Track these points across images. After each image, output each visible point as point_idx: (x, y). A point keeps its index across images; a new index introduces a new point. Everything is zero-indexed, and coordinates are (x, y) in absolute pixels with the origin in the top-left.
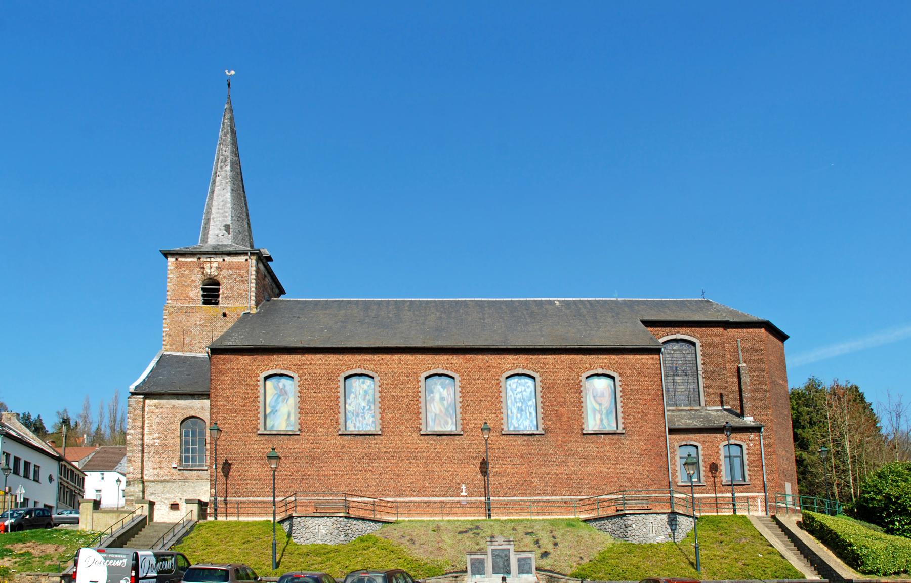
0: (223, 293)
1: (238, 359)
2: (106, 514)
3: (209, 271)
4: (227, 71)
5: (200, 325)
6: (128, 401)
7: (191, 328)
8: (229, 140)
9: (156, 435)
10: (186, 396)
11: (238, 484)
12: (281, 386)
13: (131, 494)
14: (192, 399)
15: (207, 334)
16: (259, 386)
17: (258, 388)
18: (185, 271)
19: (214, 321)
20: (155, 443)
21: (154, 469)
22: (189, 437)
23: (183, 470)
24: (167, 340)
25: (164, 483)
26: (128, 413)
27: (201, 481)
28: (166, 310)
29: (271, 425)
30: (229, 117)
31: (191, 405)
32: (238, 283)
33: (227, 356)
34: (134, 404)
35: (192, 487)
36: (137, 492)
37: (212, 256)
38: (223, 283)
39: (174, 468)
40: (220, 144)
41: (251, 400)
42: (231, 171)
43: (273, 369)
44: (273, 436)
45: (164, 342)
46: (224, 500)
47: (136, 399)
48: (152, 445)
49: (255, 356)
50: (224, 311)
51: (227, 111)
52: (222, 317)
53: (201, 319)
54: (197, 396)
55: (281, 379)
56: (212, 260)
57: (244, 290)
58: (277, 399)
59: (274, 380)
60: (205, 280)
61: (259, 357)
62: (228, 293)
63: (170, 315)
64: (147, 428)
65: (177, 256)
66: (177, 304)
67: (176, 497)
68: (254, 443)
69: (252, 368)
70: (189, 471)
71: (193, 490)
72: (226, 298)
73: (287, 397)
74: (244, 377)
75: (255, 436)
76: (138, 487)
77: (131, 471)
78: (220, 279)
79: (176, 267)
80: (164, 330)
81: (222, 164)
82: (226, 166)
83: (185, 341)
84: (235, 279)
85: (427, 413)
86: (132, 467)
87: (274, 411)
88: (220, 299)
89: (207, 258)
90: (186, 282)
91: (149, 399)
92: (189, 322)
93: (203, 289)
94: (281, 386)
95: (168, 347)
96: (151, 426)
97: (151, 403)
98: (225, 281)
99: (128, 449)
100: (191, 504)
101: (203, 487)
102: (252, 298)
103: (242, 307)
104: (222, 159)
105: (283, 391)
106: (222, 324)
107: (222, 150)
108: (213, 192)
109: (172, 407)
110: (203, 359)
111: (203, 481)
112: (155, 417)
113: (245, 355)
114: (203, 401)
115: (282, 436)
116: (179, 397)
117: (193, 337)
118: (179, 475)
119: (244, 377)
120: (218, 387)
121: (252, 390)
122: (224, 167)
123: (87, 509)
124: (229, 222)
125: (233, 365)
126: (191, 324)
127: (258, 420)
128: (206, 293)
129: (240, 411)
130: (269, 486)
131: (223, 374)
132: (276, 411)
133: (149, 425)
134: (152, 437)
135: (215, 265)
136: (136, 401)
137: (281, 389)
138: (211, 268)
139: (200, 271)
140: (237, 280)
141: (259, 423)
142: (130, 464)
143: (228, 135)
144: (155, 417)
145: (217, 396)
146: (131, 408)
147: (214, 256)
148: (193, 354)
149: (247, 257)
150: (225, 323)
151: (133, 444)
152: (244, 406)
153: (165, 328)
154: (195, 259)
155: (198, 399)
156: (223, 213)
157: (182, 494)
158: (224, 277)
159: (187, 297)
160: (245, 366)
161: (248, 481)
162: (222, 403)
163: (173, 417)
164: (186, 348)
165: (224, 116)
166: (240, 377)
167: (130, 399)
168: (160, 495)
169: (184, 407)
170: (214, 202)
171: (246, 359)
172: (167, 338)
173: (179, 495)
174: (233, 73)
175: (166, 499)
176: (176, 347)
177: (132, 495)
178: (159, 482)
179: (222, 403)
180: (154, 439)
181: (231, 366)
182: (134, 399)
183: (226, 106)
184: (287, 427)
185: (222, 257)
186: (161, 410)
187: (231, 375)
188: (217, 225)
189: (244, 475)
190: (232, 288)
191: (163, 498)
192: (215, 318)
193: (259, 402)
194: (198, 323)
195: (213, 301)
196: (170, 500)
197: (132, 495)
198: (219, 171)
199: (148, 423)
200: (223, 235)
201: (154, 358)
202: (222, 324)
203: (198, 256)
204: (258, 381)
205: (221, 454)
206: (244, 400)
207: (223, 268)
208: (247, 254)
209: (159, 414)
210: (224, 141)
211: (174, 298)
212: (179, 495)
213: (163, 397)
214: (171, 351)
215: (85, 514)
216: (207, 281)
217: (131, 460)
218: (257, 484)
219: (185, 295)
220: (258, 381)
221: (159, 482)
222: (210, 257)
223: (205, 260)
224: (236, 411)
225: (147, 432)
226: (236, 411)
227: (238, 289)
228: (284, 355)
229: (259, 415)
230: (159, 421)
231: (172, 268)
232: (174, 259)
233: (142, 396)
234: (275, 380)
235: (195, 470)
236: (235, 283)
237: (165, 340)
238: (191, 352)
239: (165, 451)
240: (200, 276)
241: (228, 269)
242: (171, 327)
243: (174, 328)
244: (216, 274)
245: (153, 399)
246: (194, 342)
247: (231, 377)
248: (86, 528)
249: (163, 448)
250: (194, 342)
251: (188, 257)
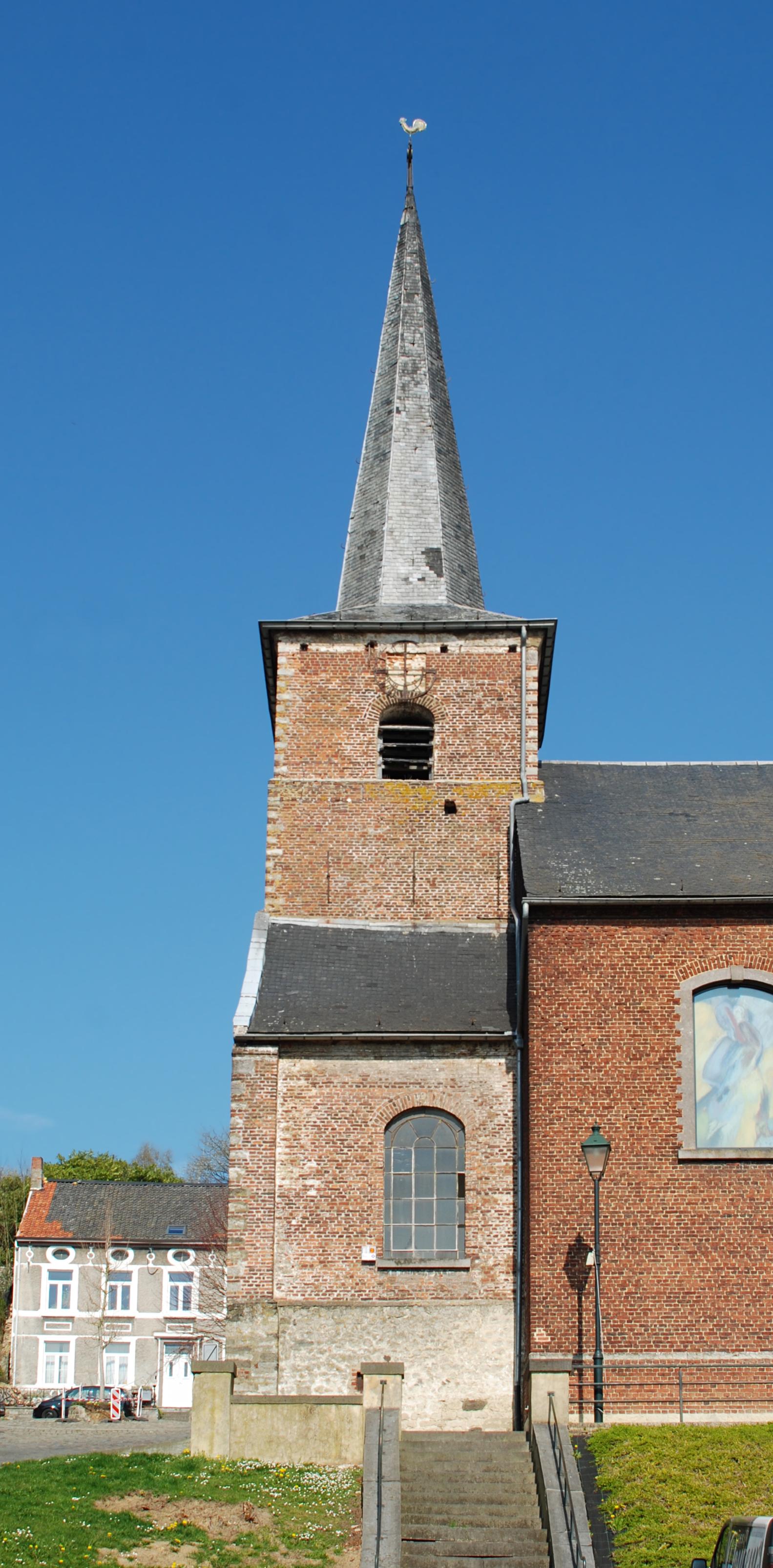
0: (443, 744)
1: (612, 936)
2: (270, 1406)
3: (399, 681)
4: (403, 120)
5: (378, 838)
6: (234, 1065)
7: (351, 846)
8: (421, 310)
9: (309, 1164)
10: (404, 1047)
11: (618, 1312)
12: (739, 1017)
13: (241, 1344)
14: (422, 1057)
15: (397, 864)
16: (677, 1017)
17: (676, 1023)
18: (328, 681)
19: (420, 827)
20: (306, 1188)
21: (304, 1266)
22: (410, 1170)
23: (394, 1269)
24: (277, 884)
25: (338, 1310)
26: (234, 1099)
27: (449, 1302)
28: (276, 793)
29: (711, 1133)
30: (416, 248)
31: (417, 1075)
32: (487, 716)
33: (578, 928)
34: (252, 1072)
35: (423, 1320)
36: (262, 1340)
37: (410, 637)
38: (443, 716)
39: (365, 1263)
41: (654, 1058)
42: (432, 397)
43: (721, 967)
44: (722, 1166)
45: (269, 889)
46: (574, 1362)
47: (258, 1058)
48: (297, 1195)
49: (664, 929)
50: (448, 796)
51: (409, 232)
53: (380, 819)
54: (440, 1047)
55: (738, 996)
56: (411, 648)
57: (507, 737)
58: (729, 1053)
59: (720, 997)
60: (387, 707)
61: (678, 932)
62: (457, 744)
63: (287, 807)
64: (283, 1143)
65: (306, 640)
66: (304, 775)
67: (375, 1351)
68: (666, 1188)
69: (655, 965)
70: (411, 1274)
71: (427, 1329)
72: (451, 758)
73: (758, 1050)
74: (633, 991)
75: (668, 1165)
76: (265, 1322)
77: (242, 1274)
78: (433, 703)
79: (303, 671)
80: (269, 852)
81: (407, 378)
82: (417, 384)
83: (333, 884)
84: (480, 703)
86: (245, 1263)
87: (720, 1092)
88: (435, 760)
89: (394, 644)
91: (289, 1057)
92: (344, 828)
93: (385, 735)
94: (739, 1017)
95: (281, 901)
96: (296, 1138)
97: (295, 1070)
98: (449, 709)
99: (232, 1207)
100: (549, 1375)
101: (457, 1323)
103: (504, 786)
104: (406, 364)
105: (745, 1030)
106: (444, 833)
107: (403, 339)
108: (383, 456)
109: (357, 1079)
110: (391, 938)
111: (455, 1302)
112: (306, 1111)
114: (456, 1060)
115: (751, 1166)
116: (383, 1050)
117: (356, 872)
118: (380, 1284)
119: (633, 991)
120: (555, 1020)
121: (656, 1028)
122: (412, 385)
123: (213, 1391)
124: (436, 541)
125: (597, 954)
126: (351, 835)
127: (677, 1119)
129: (622, 1092)
130: (712, 1318)
131: (569, 982)
132: (727, 1091)
133: (288, 1136)
134: (297, 1171)
135: (418, 663)
136: (256, 1062)
137: (741, 1025)
138: (406, 670)
139: (374, 680)
140: (486, 705)
141: (680, 1127)
142: (239, 1253)
143: (417, 298)
144: (306, 1111)
145: (551, 1045)
146: (243, 1085)
147: (415, 637)
148: (357, 924)
150: (453, 832)
151: (248, 1194)
152: (635, 1076)
153: (270, 846)
154: (358, 647)
155: (438, 1057)
156: (417, 516)
157: (393, 1344)
158: (447, 699)
159: (336, 756)
161: (649, 1303)
162: (565, 1067)
163: (364, 1110)
165: (402, 244)
166: (620, 989)
167: (238, 1058)
168: (325, 1347)
169: (397, 1080)
171: (637, 937)
172: (279, 877)
173: (384, 1345)
174: (420, 124)
175: (344, 1358)
176: (306, 904)
177: (248, 1349)
178: (322, 1306)
179: (565, 1067)
180: (303, 1177)
181: (591, 957)
182: (253, 1058)
183: (405, 218)
184: (758, 1137)
185: (439, 640)
186: (326, 1090)
188: (402, 549)
189: (637, 1285)
190: (469, 731)
191: (333, 1357)
192: (421, 816)
193: (680, 1066)
194: (371, 831)
195: (414, 768)
196: (356, 1362)
197: (248, 1349)
198: (399, 398)
199: (287, 1129)
200: (422, 579)
201: (250, 937)
202: (444, 833)
203: (370, 637)
204: (677, 1002)
205: (565, 1222)
206: (634, 1058)
207: (443, 673)
208: (517, 631)
209: (318, 1100)
211: (297, 760)
212: (384, 1345)
213: (333, 1048)
215: (209, 1407)
216: (391, 709)
217: (241, 1240)
218: (676, 1310)
219: (329, 752)
220: (677, 1002)
221: (322, 1306)
222: (405, 642)
224: (608, 1092)
225: (284, 1157)
226: (608, 1092)
227: (488, 733)
228: (753, 924)
229: (679, 1105)
230: (318, 1123)
231: (291, 672)
232: (295, 648)
234: (720, 998)
235: (431, 1269)
236: (480, 716)
237: (272, 883)
238: (351, 915)
239: (339, 1212)
240: (373, 696)
241: (456, 677)
242: (290, 844)
243: (299, 846)
244: (422, 690)
245: (300, 1057)
246: (359, 886)
247: (591, 989)
248: (211, 1451)
249: (332, 1205)
250: (359, 886)
251: (339, 641)
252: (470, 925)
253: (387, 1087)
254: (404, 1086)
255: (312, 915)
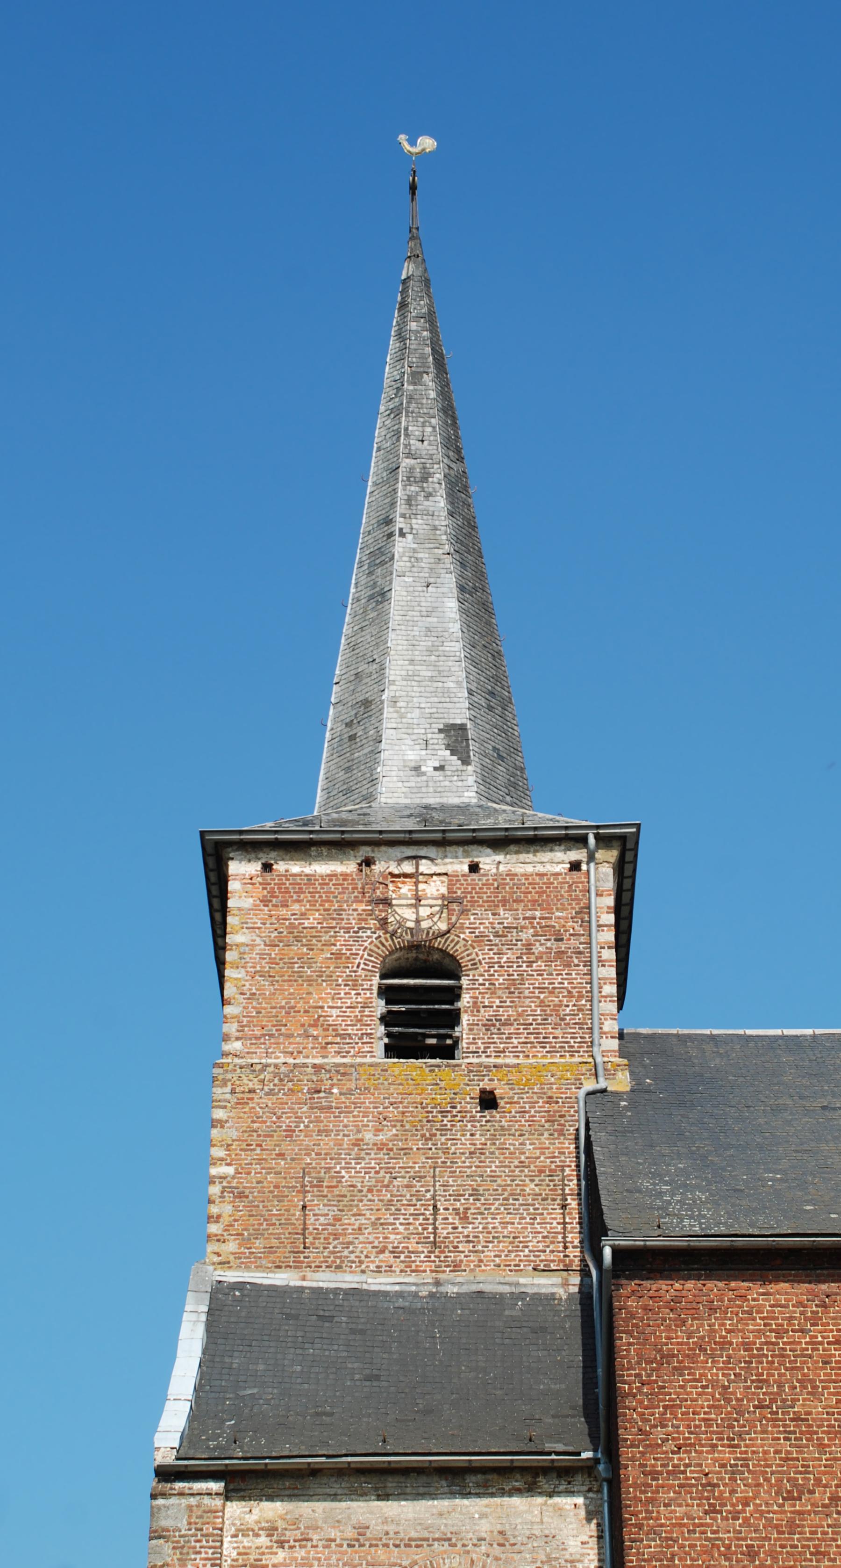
0: (476, 1006)
1: (743, 1297)
3: (409, 914)
4: (402, 138)
5: (380, 1147)
6: (154, 1513)
7: (338, 1162)
8: (432, 394)
10: (423, 1479)
14: (452, 1495)
19: (443, 1130)
24: (226, 1219)
28: (225, 1083)
30: (425, 310)
31: (446, 1526)
33: (690, 1285)
34: (183, 1524)
37: (423, 851)
40: (396, 412)
42: (451, 514)
45: (213, 1228)
47: (193, 1501)
49: (824, 1287)
50: (486, 1084)
52: (474, 1109)
53: (382, 1120)
56: (425, 867)
60: (391, 953)
63: (240, 1103)
65: (270, 856)
66: (268, 1055)
72: (488, 1026)
74: (781, 1386)
79: (265, 901)
80: (214, 1171)
82: (428, 496)
83: (311, 1220)
84: (529, 946)
85: (187, 1456)
88: (463, 1030)
89: (400, 861)
90: (310, 962)
91: (243, 1498)
92: (327, 1132)
93: (388, 993)
95: (232, 1246)
97: (251, 1519)
98: (483, 955)
102: (606, 1028)
103: (568, 1067)
104: (412, 469)
106: (479, 1139)
107: (407, 435)
109: (350, 1533)
110: (400, 1302)
113: (777, 1280)
114: (506, 1500)
116: (391, 1483)
119: (781, 1386)
121: (821, 1446)
122: (421, 498)
124: (460, 714)
126: (339, 1144)
128: (395, 1008)
131: (679, 1370)
135: (435, 888)
136: (190, 1508)
140: (538, 949)
145: (655, 1474)
146: (167, 1548)
147: (431, 851)
148: (348, 1280)
149: (575, 855)
152: (792, 1527)
153: (215, 1162)
154: (347, 866)
155: (478, 1495)
159: (315, 1025)
160: (779, 1333)
162: (680, 1511)
164: (312, 1254)
165: (403, 305)
166: (761, 1382)
167: (160, 1502)
170: (391, 635)
171: (782, 1299)
172: (228, 1209)
174: (427, 143)
176: (270, 1250)
179: (680, 1511)
182: (184, 1502)
183: (408, 269)
185: (467, 854)
186: (300, 1553)
187: (714, 1372)
194: (368, 1136)
195: (433, 1041)
198: (403, 516)
200: (441, 768)
202: (479, 1139)
203: (365, 851)
206: (790, 1497)
207: (472, 902)
210: (411, 398)
214: (247, 1268)
219: (304, 1019)
223: (394, 869)
227: (542, 989)
232: (253, 868)
233: (216, 1486)
236: (530, 963)
241: (493, 907)
242: (245, 1157)
244: (443, 926)
247: (714, 1383)
251: (319, 858)
252: (522, 1281)
253: (397, 1546)
254: (425, 1543)
255: (279, 1267)
